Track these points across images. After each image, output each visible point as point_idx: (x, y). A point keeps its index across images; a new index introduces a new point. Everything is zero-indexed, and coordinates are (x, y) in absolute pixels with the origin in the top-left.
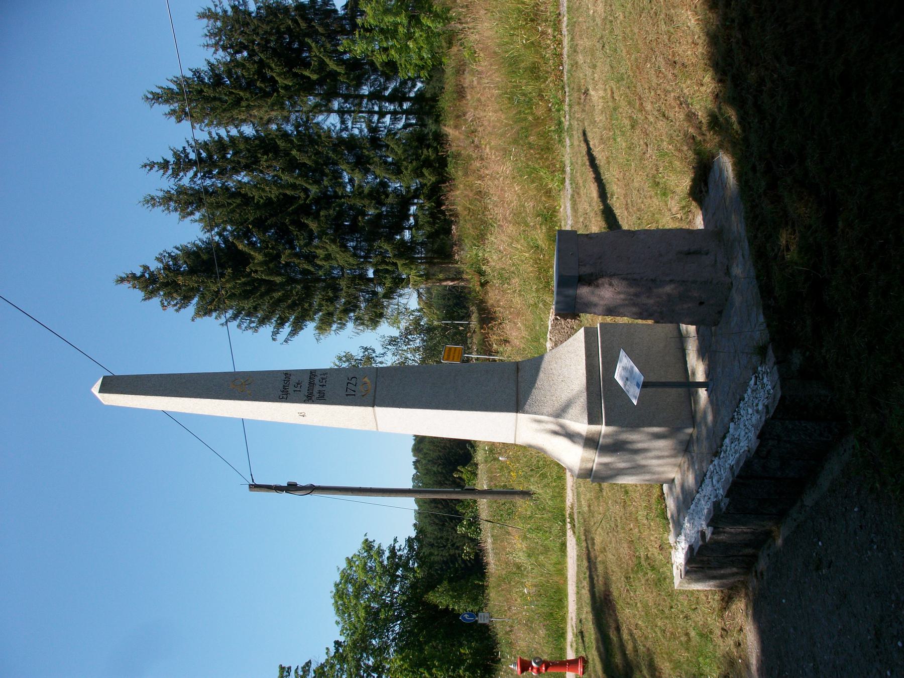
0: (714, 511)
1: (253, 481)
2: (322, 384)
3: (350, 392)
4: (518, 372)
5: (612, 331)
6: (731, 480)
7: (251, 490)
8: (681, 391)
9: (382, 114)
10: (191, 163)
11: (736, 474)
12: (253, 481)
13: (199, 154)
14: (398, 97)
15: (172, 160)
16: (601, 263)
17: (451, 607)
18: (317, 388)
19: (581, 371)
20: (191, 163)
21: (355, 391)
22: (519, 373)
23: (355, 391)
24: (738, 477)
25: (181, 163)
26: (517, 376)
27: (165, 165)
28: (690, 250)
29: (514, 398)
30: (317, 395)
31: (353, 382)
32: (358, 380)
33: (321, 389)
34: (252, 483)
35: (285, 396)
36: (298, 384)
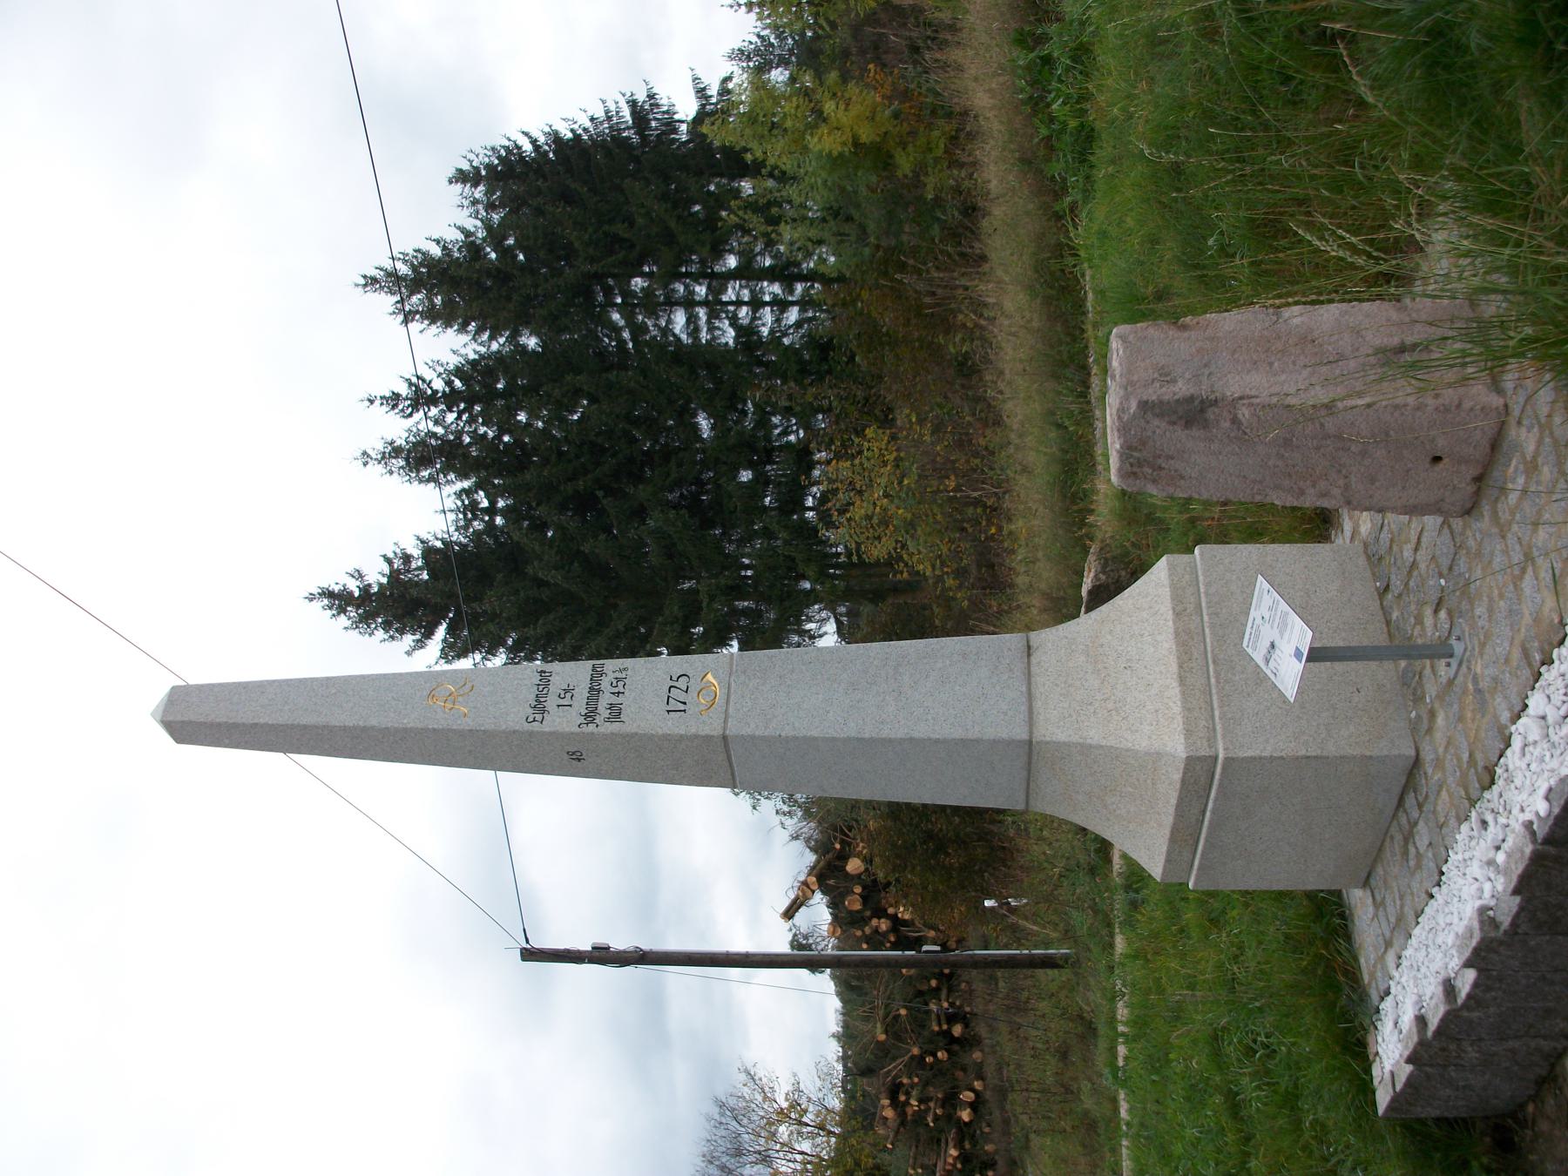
0: (1481, 929)
1: (527, 941)
2: (616, 690)
3: (674, 705)
4: (1029, 655)
5: (1227, 561)
6: (1528, 850)
7: (523, 960)
8: (1384, 672)
9: (756, 304)
10: (432, 400)
11: (1540, 835)
12: (527, 941)
13: (449, 383)
14: (785, 273)
15: (404, 390)
16: (1210, 374)
17: (685, 174)
18: (605, 700)
19: (1166, 645)
20: (432, 400)
21: (685, 703)
22: (1032, 658)
23: (685, 703)
24: (1548, 840)
25: (421, 398)
26: (1029, 663)
27: (394, 400)
28: (1403, 343)
29: (1024, 708)
30: (606, 713)
31: (682, 683)
32: (692, 681)
33: (614, 699)
34: (525, 945)
35: (539, 717)
36: (566, 691)
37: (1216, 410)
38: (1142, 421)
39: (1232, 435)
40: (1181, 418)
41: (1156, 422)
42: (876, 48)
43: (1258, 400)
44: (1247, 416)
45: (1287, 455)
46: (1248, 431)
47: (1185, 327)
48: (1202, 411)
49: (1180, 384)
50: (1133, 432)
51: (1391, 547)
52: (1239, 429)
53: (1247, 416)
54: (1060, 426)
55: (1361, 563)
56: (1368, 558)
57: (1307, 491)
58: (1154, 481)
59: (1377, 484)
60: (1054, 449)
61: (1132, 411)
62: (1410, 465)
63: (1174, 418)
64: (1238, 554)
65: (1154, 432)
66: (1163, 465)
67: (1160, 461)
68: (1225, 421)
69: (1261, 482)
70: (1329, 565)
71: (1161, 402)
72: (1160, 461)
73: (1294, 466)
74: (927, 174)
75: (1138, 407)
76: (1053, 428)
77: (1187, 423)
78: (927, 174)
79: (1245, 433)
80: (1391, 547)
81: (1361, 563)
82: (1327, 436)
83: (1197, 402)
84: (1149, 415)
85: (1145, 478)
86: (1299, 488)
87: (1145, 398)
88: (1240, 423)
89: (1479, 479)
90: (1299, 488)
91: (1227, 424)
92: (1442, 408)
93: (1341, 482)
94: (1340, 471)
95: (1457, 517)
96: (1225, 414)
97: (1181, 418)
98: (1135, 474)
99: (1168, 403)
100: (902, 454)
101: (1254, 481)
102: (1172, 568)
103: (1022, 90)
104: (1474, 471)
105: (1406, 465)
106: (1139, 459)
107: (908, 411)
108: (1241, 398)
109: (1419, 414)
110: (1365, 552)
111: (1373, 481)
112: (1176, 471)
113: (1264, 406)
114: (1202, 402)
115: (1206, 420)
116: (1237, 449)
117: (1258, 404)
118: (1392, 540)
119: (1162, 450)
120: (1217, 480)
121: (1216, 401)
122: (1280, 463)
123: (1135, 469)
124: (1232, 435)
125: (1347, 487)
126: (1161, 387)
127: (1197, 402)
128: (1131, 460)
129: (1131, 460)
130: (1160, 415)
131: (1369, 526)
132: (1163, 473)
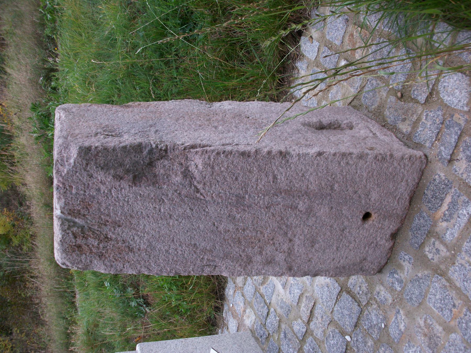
16: (157, 131)
37: (166, 162)
38: (85, 174)
39: (184, 192)
40: (128, 171)
41: (100, 176)
42: (8, 204)
43: (212, 148)
44: (200, 167)
45: (238, 216)
46: (200, 186)
47: (128, 107)
48: (151, 164)
49: (126, 137)
50: (74, 191)
51: (279, 326)
52: (191, 184)
53: (200, 167)
54: (64, 318)
55: (252, 344)
56: (257, 339)
57: (254, 259)
58: (101, 256)
59: (317, 246)
60: (62, 328)
61: (72, 161)
62: (346, 223)
63: (120, 171)
64: (168, 347)
65: (99, 190)
66: (110, 235)
67: (106, 230)
68: (176, 175)
69: (211, 251)
70: (232, 347)
71: (106, 149)
72: (106, 230)
73: (244, 230)
74: (24, 245)
75: (79, 154)
76: (61, 319)
77: (135, 177)
78: (24, 245)
79: (198, 191)
80: (279, 326)
81: (252, 344)
82: (278, 192)
83: (145, 152)
84: (92, 168)
85: (91, 252)
86: (247, 256)
87: (87, 144)
88: (192, 177)
89: (394, 236)
90: (247, 256)
91: (178, 179)
92: (380, 157)
93: (285, 247)
94: (286, 234)
95: (374, 274)
96: (176, 166)
97: (128, 171)
98: (79, 247)
99: (114, 149)
100: (14, 345)
101: (204, 251)
102: (140, 345)
103: (34, 132)
104: (391, 227)
105: (343, 223)
106: (83, 227)
107: (16, 329)
108: (193, 147)
109: (361, 162)
110: (254, 336)
111: (313, 242)
112: (124, 242)
113: (218, 154)
114: (151, 152)
115: (155, 176)
116: (188, 211)
117: (213, 151)
118: (280, 321)
119: (108, 215)
120: (167, 251)
121: (166, 151)
122: (231, 227)
123: (79, 241)
124: (184, 192)
125: (290, 252)
126: (105, 138)
127: (145, 152)
128: (75, 229)
129: (75, 229)
130: (105, 167)
131: (254, 317)
132: (110, 245)
